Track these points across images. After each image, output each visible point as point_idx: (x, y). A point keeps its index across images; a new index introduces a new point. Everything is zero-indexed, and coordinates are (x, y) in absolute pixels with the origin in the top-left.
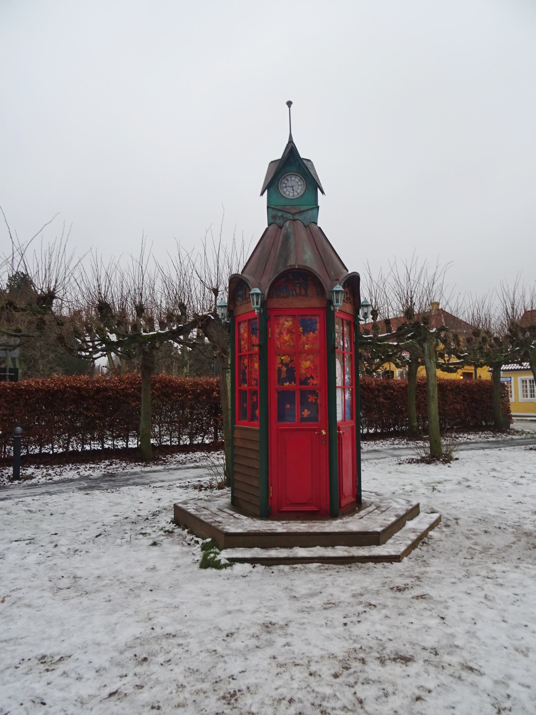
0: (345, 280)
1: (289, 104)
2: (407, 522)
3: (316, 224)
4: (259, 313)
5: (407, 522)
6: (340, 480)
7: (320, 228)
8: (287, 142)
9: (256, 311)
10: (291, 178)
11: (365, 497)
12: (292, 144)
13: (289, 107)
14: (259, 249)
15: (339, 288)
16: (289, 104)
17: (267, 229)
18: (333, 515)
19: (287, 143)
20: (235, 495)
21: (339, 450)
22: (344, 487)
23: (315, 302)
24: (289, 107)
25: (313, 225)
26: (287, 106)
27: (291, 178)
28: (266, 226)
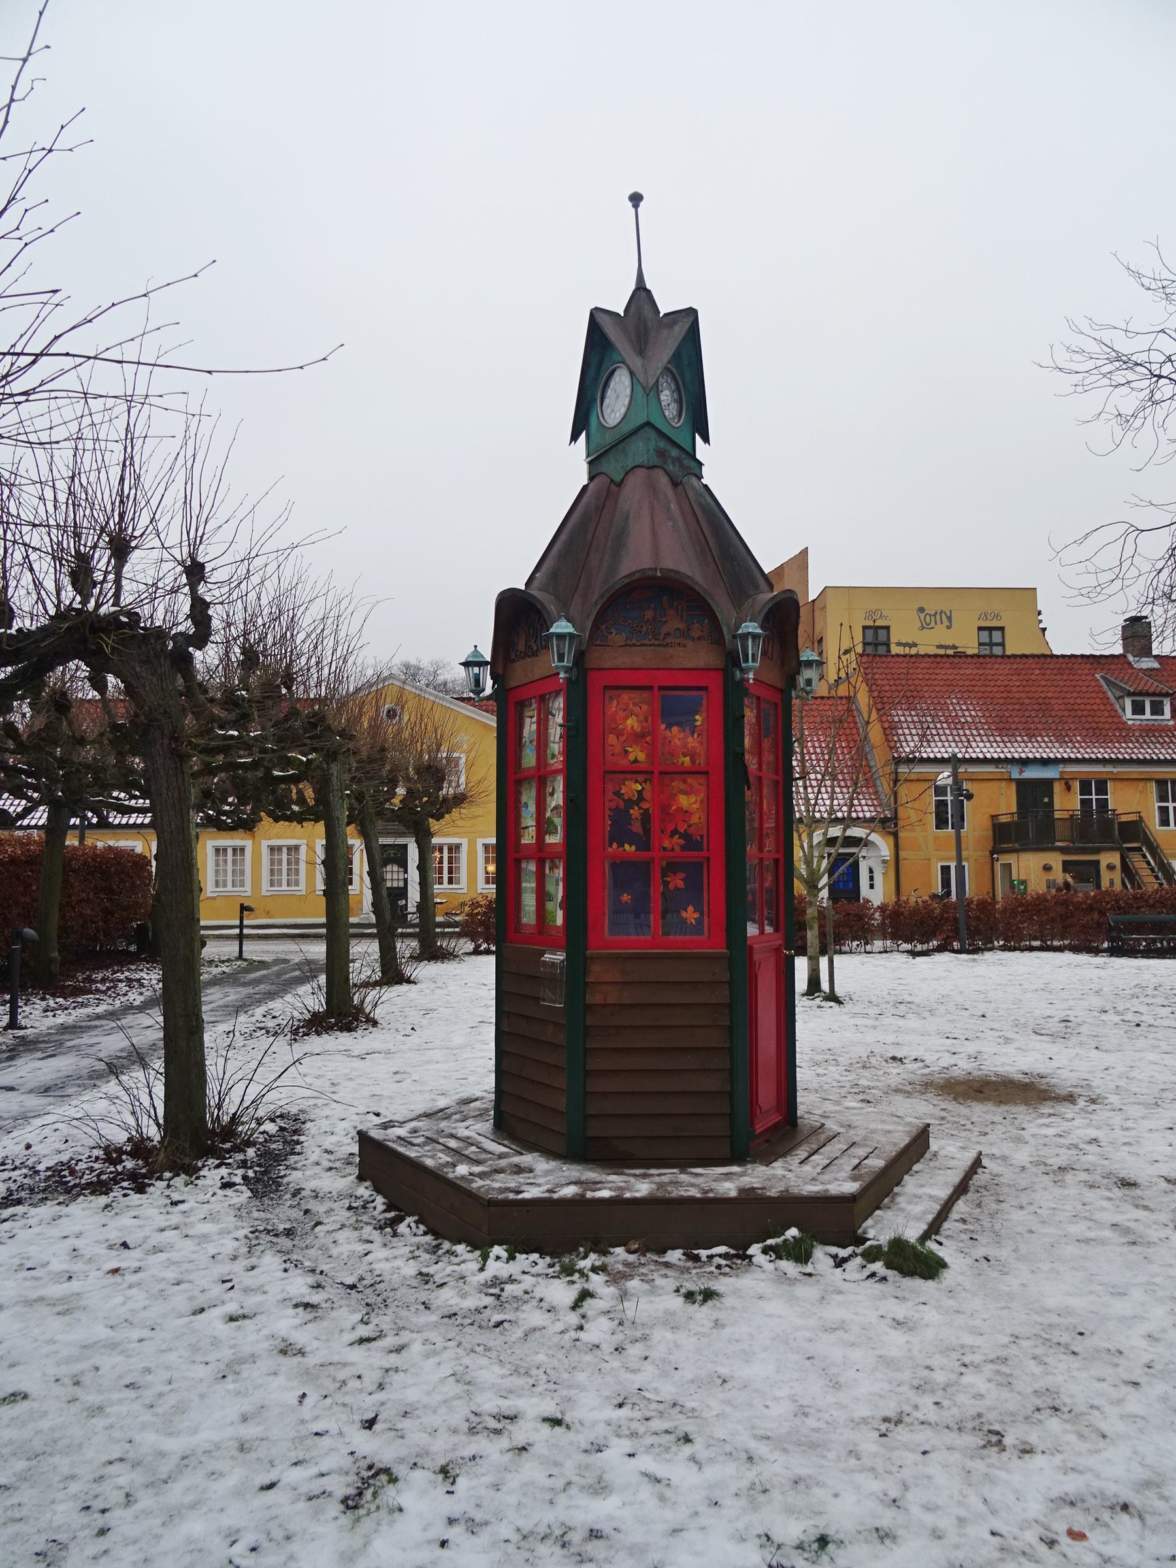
0: (770, 605)
1: (636, 199)
2: (663, 311)
3: (700, 477)
4: (568, 680)
5: (663, 311)
6: (751, 1058)
7: (706, 486)
8: (633, 287)
9: (562, 675)
10: (644, 366)
11: (805, 1102)
12: (643, 294)
13: (636, 206)
14: (563, 537)
15: (752, 627)
16: (636, 199)
17: (585, 488)
18: (739, 1156)
19: (633, 288)
20: (502, 1108)
21: (751, 1051)
22: (759, 1059)
23: (697, 656)
24: (636, 206)
25: (694, 480)
26: (630, 204)
27: (644, 366)
28: (585, 481)
